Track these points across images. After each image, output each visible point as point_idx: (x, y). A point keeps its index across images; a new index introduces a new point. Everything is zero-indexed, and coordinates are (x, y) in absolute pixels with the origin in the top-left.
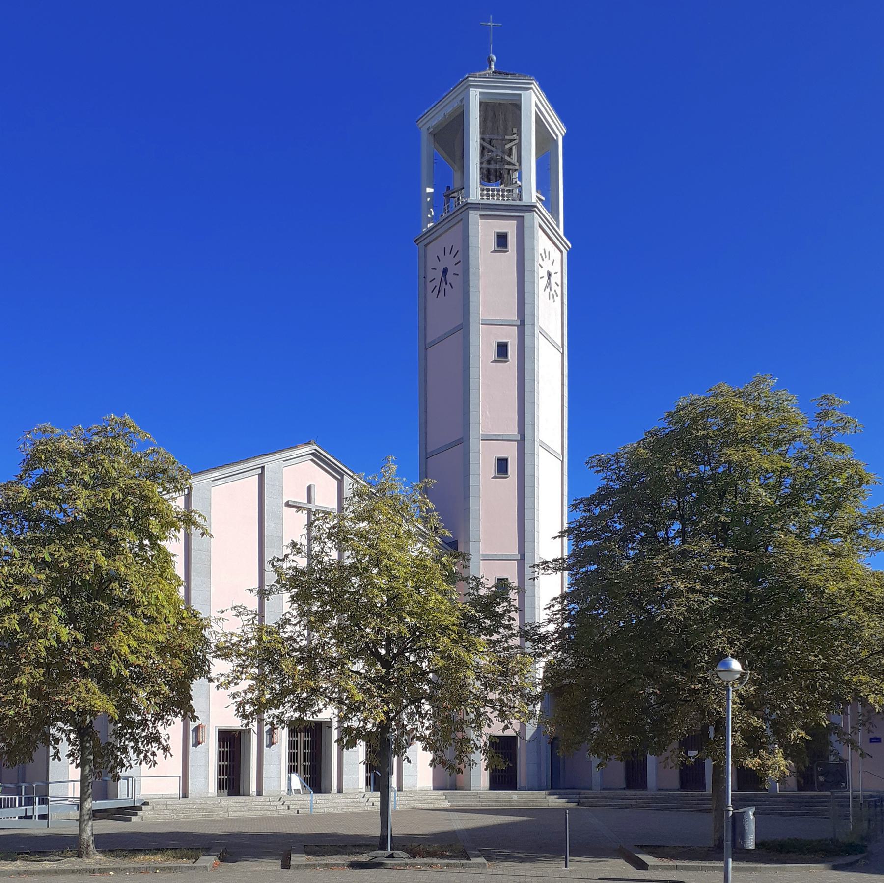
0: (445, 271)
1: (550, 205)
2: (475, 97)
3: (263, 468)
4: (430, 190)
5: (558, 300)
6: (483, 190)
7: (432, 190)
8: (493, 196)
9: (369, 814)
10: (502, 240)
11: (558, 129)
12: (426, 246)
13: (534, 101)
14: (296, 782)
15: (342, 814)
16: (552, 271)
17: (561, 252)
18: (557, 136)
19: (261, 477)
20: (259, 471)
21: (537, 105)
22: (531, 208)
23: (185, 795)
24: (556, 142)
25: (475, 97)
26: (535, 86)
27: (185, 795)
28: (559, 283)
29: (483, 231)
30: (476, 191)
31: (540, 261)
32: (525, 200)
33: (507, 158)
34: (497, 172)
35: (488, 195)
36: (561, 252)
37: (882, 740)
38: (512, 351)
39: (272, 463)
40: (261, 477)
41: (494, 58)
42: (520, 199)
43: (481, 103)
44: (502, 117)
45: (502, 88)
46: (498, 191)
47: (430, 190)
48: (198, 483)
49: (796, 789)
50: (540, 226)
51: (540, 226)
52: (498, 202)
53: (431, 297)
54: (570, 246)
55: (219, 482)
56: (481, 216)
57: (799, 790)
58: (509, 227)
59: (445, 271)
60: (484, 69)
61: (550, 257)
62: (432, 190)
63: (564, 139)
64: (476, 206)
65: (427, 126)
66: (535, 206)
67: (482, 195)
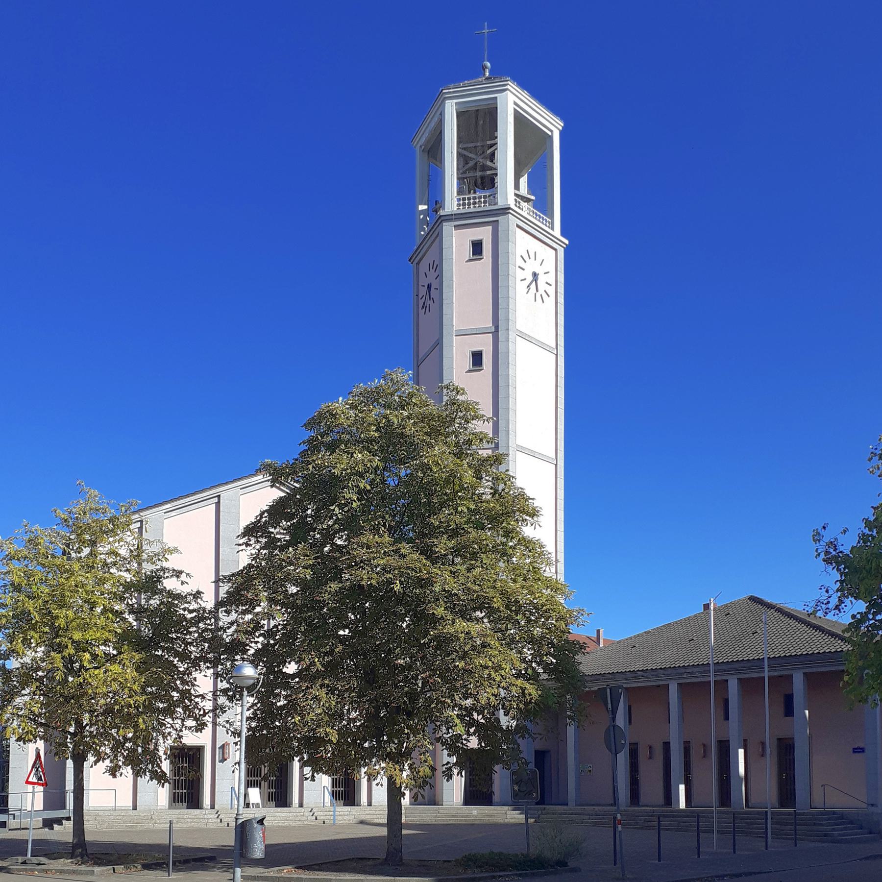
0: (429, 286)
1: (543, 205)
2: (450, 110)
3: (219, 496)
4: (422, 207)
5: (550, 302)
6: (459, 200)
7: (426, 207)
8: (469, 204)
9: (69, 832)
10: (477, 247)
11: (552, 125)
12: (418, 264)
13: (512, 100)
14: (255, 795)
15: (286, 827)
16: (540, 271)
17: (556, 250)
18: (551, 131)
19: (218, 504)
20: (216, 500)
21: (515, 103)
22: (505, 211)
23: (135, 808)
24: (551, 138)
25: (450, 110)
26: (512, 86)
27: (135, 808)
28: (553, 283)
29: (457, 241)
30: (451, 203)
31: (520, 262)
32: (501, 203)
33: (489, 163)
34: (480, 177)
35: (464, 204)
36: (556, 250)
37: (866, 751)
38: (487, 360)
39: (228, 493)
40: (218, 504)
41: (489, 64)
42: (496, 204)
43: (457, 113)
44: (480, 124)
45: (474, 94)
46: (469, 199)
47: (422, 207)
48: (149, 515)
49: (777, 805)
50: (518, 226)
51: (518, 226)
52: (464, 211)
53: (422, 311)
54: (567, 242)
55: (173, 513)
56: (455, 226)
57: (782, 806)
58: (484, 234)
59: (429, 286)
60: (477, 76)
61: (536, 259)
62: (426, 207)
63: (562, 134)
64: (451, 218)
65: (419, 145)
66: (509, 208)
67: (459, 205)
